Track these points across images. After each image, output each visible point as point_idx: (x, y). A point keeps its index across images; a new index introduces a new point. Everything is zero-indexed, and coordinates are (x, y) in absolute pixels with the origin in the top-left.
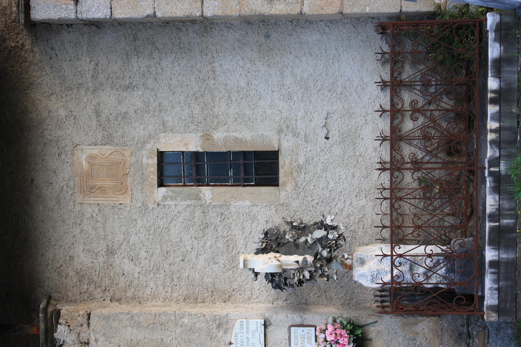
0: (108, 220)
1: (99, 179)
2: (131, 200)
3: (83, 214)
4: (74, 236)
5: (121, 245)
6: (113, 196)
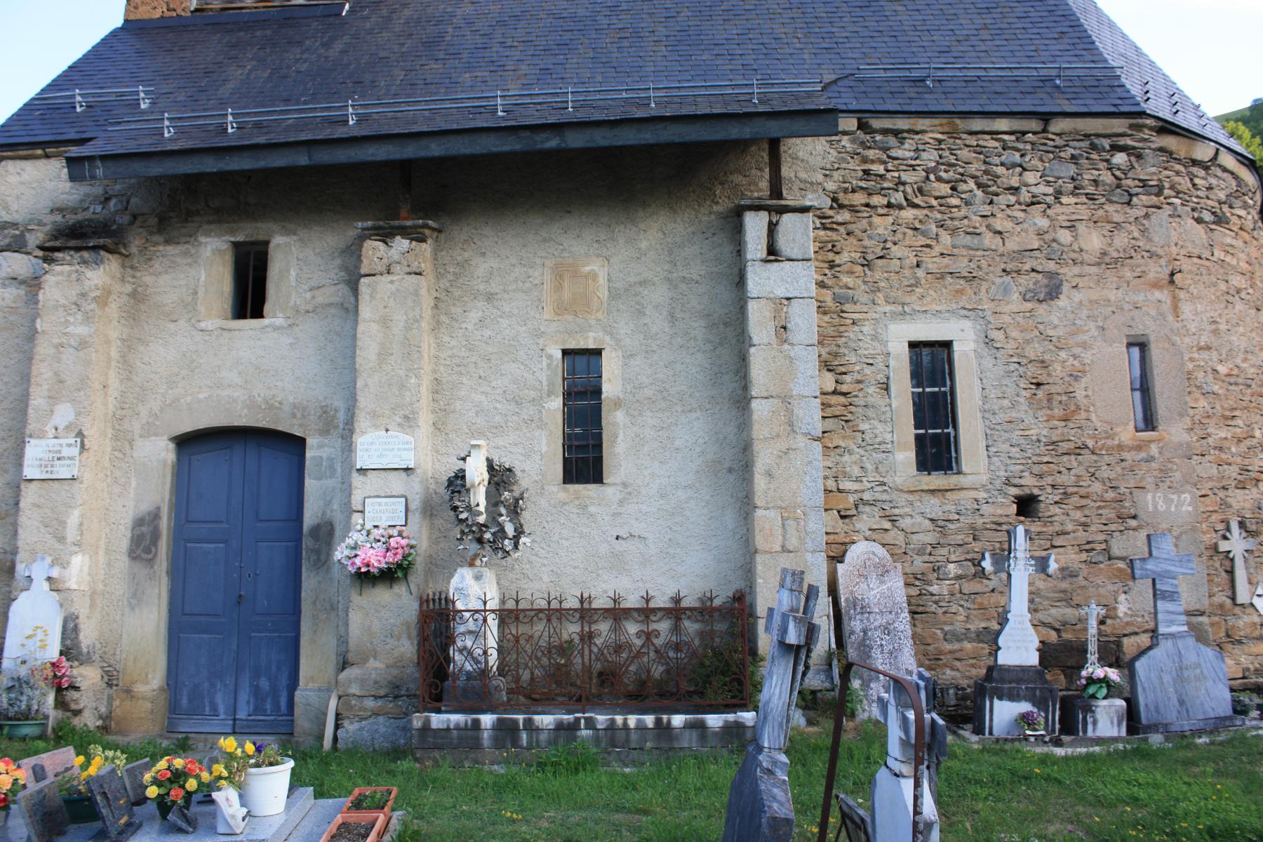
4: (507, 257)
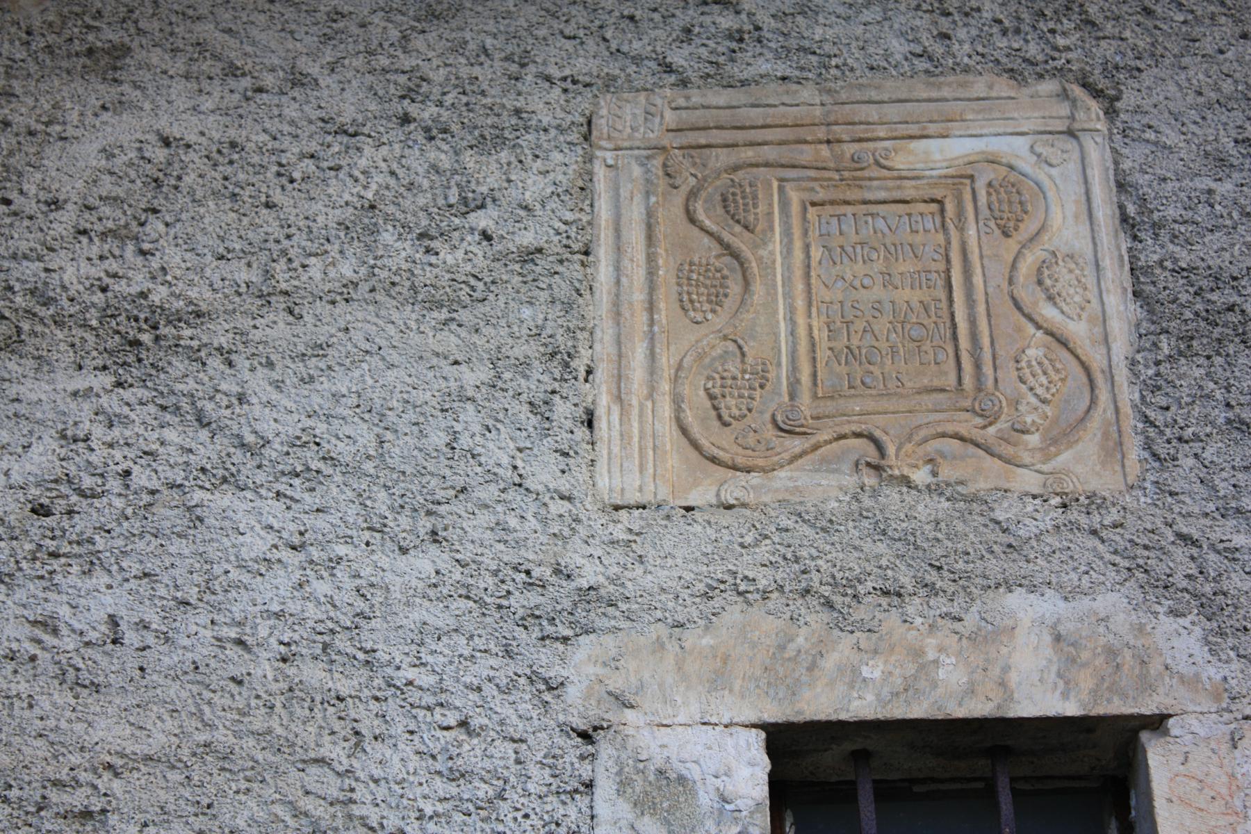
0: (444, 314)
1: (816, 253)
2: (633, 497)
3: (500, 141)
4: (298, 80)
5: (202, 421)
6: (666, 361)
